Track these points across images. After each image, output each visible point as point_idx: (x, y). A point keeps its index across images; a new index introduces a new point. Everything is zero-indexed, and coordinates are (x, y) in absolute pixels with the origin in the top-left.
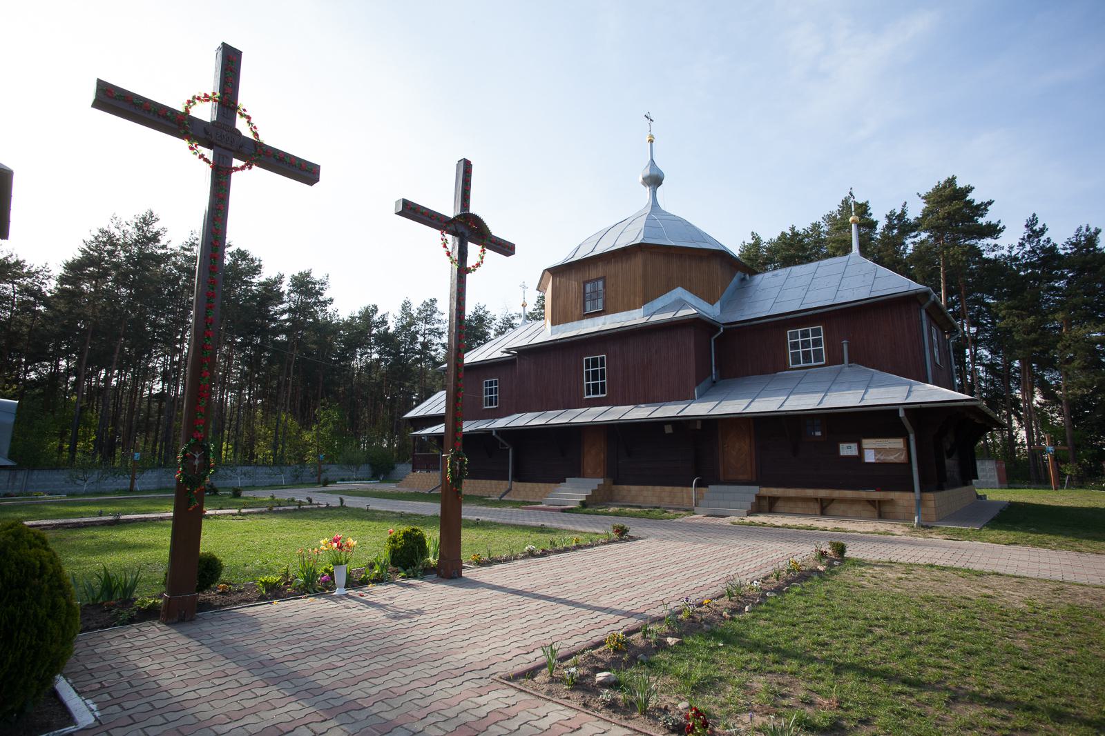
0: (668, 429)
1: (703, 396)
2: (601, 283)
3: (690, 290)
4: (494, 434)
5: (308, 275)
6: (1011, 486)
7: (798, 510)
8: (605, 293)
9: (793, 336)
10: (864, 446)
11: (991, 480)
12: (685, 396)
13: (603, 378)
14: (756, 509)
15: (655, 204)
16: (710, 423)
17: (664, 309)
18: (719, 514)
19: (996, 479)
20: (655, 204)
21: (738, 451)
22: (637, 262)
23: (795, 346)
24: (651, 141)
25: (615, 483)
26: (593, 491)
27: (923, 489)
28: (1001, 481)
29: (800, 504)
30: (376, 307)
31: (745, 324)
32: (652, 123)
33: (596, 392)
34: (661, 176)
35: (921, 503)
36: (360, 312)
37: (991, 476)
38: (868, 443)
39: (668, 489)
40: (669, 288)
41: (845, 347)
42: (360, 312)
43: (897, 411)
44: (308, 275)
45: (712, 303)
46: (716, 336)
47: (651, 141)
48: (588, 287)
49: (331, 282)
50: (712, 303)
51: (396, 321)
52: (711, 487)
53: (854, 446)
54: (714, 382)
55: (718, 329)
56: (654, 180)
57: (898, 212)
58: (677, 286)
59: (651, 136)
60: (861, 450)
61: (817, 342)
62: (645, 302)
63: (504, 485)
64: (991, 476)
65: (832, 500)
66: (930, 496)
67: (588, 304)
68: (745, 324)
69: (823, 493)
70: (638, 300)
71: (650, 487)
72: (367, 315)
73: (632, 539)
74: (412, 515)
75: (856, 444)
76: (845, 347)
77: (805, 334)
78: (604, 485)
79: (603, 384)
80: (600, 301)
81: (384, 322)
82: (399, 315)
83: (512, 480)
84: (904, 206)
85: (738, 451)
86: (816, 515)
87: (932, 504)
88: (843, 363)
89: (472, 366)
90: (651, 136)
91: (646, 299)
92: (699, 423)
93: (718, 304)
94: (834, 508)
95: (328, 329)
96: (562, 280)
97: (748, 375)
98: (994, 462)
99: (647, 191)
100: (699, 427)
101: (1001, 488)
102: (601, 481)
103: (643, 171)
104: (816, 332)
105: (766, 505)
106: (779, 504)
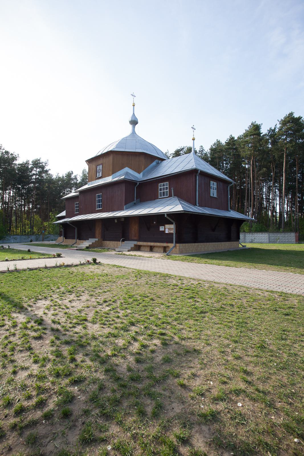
1: (127, 208)
3: (131, 168)
4: (166, 216)
5: (39, 160)
6: (300, 242)
7: (146, 250)
8: (102, 170)
9: (161, 186)
10: (166, 227)
11: (293, 240)
12: (121, 209)
14: (132, 249)
15: (134, 132)
16: (128, 219)
17: (120, 176)
19: (294, 240)
20: (134, 132)
21: (134, 229)
22: (111, 158)
23: (161, 189)
24: (134, 106)
25: (103, 240)
26: (92, 243)
27: (176, 242)
28: (296, 241)
29: (147, 248)
30: (72, 172)
31: (151, 180)
32: (135, 98)
34: (137, 120)
35: (175, 246)
36: (66, 174)
37: (293, 239)
38: (167, 226)
39: (116, 242)
40: (122, 168)
41: (172, 190)
42: (66, 174)
43: (164, 215)
44: (39, 160)
46: (136, 186)
47: (134, 106)
49: (49, 163)
50: (139, 173)
51: (80, 177)
54: (135, 203)
55: (137, 183)
56: (134, 122)
57: (273, 128)
58: (126, 167)
59: (134, 103)
60: (165, 229)
61: (161, 189)
62: (113, 173)
63: (74, 241)
64: (293, 239)
65: (154, 246)
66: (178, 245)
68: (151, 180)
69: (152, 244)
70: (111, 173)
71: (112, 242)
72: (69, 175)
73: (62, 257)
74: (22, 250)
76: (172, 190)
77: (164, 185)
78: (98, 241)
81: (76, 178)
82: (81, 175)
83: (77, 239)
84: (276, 126)
85: (134, 229)
86: (147, 251)
87: (178, 248)
88: (172, 197)
89: (74, 197)
90: (134, 103)
91: (114, 172)
92: (124, 219)
93: (142, 174)
94: (155, 249)
95: (51, 181)
96: (91, 165)
97: (147, 201)
98: (295, 233)
99: (131, 126)
101: (296, 243)
103: (129, 118)
105: (138, 248)
106: (142, 248)
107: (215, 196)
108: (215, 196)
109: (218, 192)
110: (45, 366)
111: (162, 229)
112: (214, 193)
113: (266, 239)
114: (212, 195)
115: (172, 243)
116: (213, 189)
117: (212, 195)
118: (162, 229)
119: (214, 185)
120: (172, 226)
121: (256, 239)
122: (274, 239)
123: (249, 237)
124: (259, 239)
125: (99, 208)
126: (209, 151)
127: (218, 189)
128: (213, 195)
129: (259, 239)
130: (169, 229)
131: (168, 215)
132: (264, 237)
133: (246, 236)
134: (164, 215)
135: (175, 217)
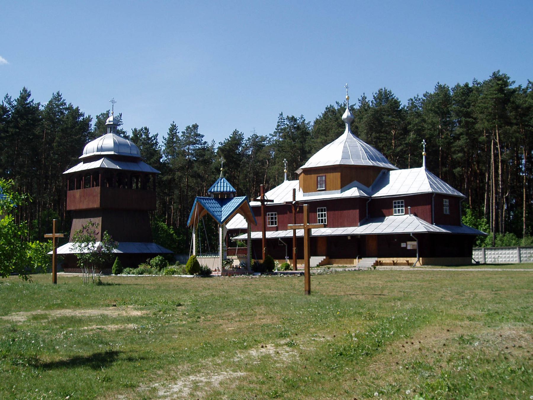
0: (349, 238)
2: (324, 177)
4: (411, 235)
8: (317, 183)
13: (325, 217)
18: (493, 266)
33: (272, 224)
38: (409, 243)
45: (368, 187)
48: (319, 178)
52: (363, 259)
53: (405, 244)
58: (354, 180)
60: (407, 245)
67: (319, 185)
75: (57, 253)
79: (325, 219)
80: (324, 185)
93: (371, 187)
100: (349, 238)
102: (325, 257)
104: (402, 202)
107: (448, 213)
108: (448, 213)
109: (450, 209)
110: (56, 324)
111: (403, 245)
112: (446, 210)
113: (516, 257)
114: (445, 213)
115: (416, 257)
116: (446, 207)
117: (445, 213)
118: (403, 245)
119: (446, 202)
120: (415, 243)
121: (501, 257)
122: (526, 256)
123: (490, 254)
124: (505, 257)
125: (319, 223)
126: (312, 124)
127: (450, 205)
128: (446, 212)
129: (505, 257)
130: (411, 245)
131: (413, 234)
132: (512, 253)
133: (486, 253)
134: (410, 234)
135: (418, 236)
